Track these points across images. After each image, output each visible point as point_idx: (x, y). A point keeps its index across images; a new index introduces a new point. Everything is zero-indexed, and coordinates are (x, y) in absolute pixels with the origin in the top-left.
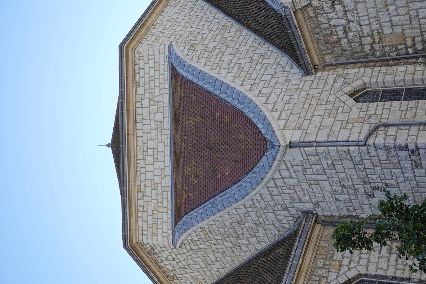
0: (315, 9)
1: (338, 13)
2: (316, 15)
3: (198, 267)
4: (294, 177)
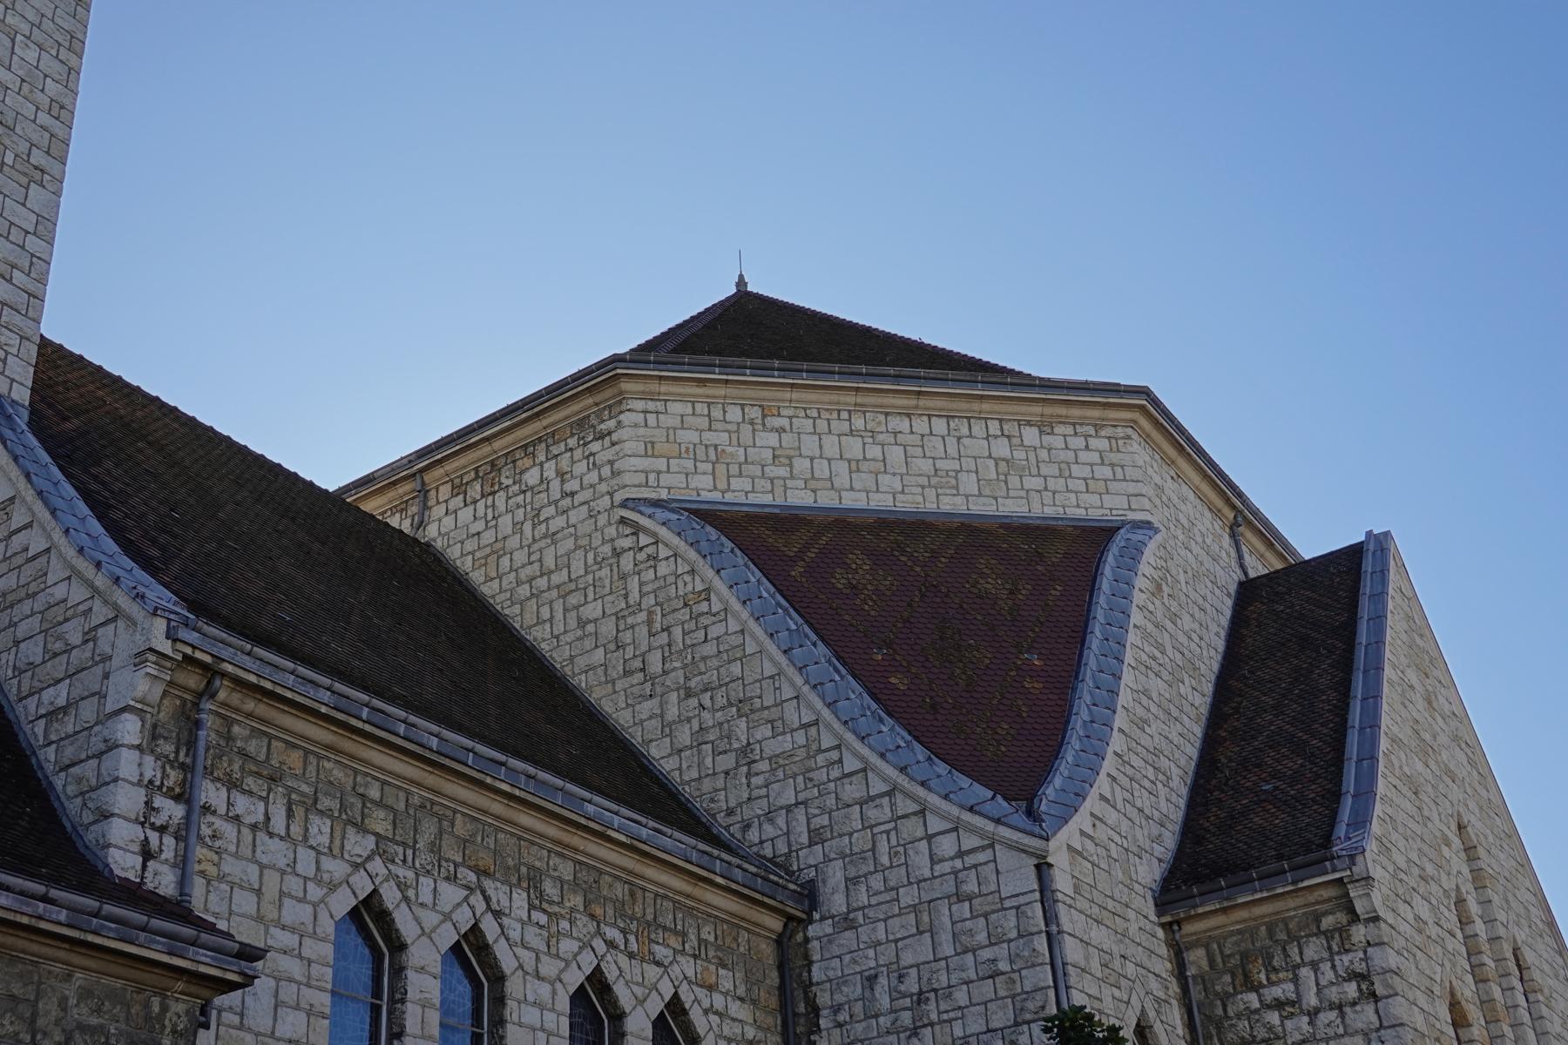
0: (1343, 931)
1: (1334, 989)
2: (1324, 933)
3: (550, 562)
4: (937, 867)
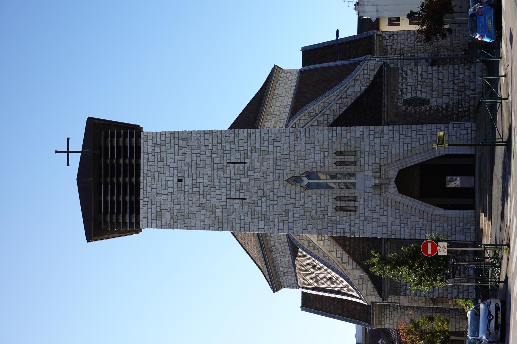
0: (383, 37)
